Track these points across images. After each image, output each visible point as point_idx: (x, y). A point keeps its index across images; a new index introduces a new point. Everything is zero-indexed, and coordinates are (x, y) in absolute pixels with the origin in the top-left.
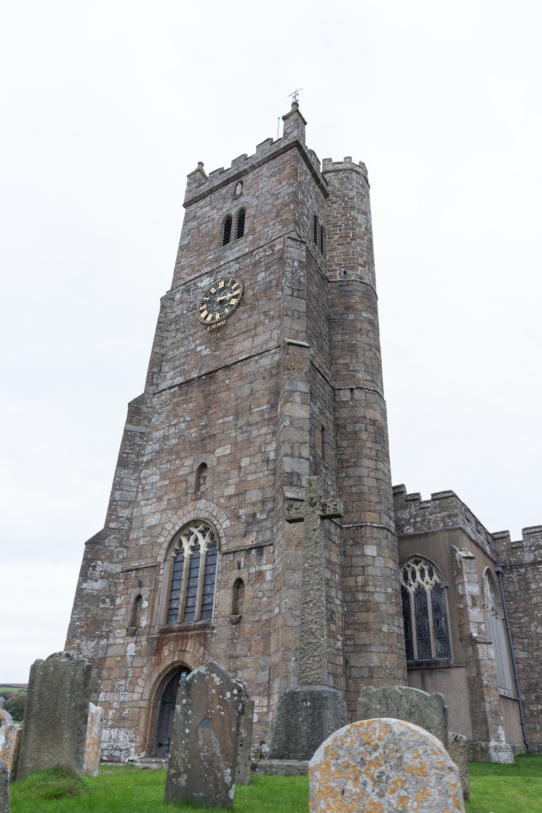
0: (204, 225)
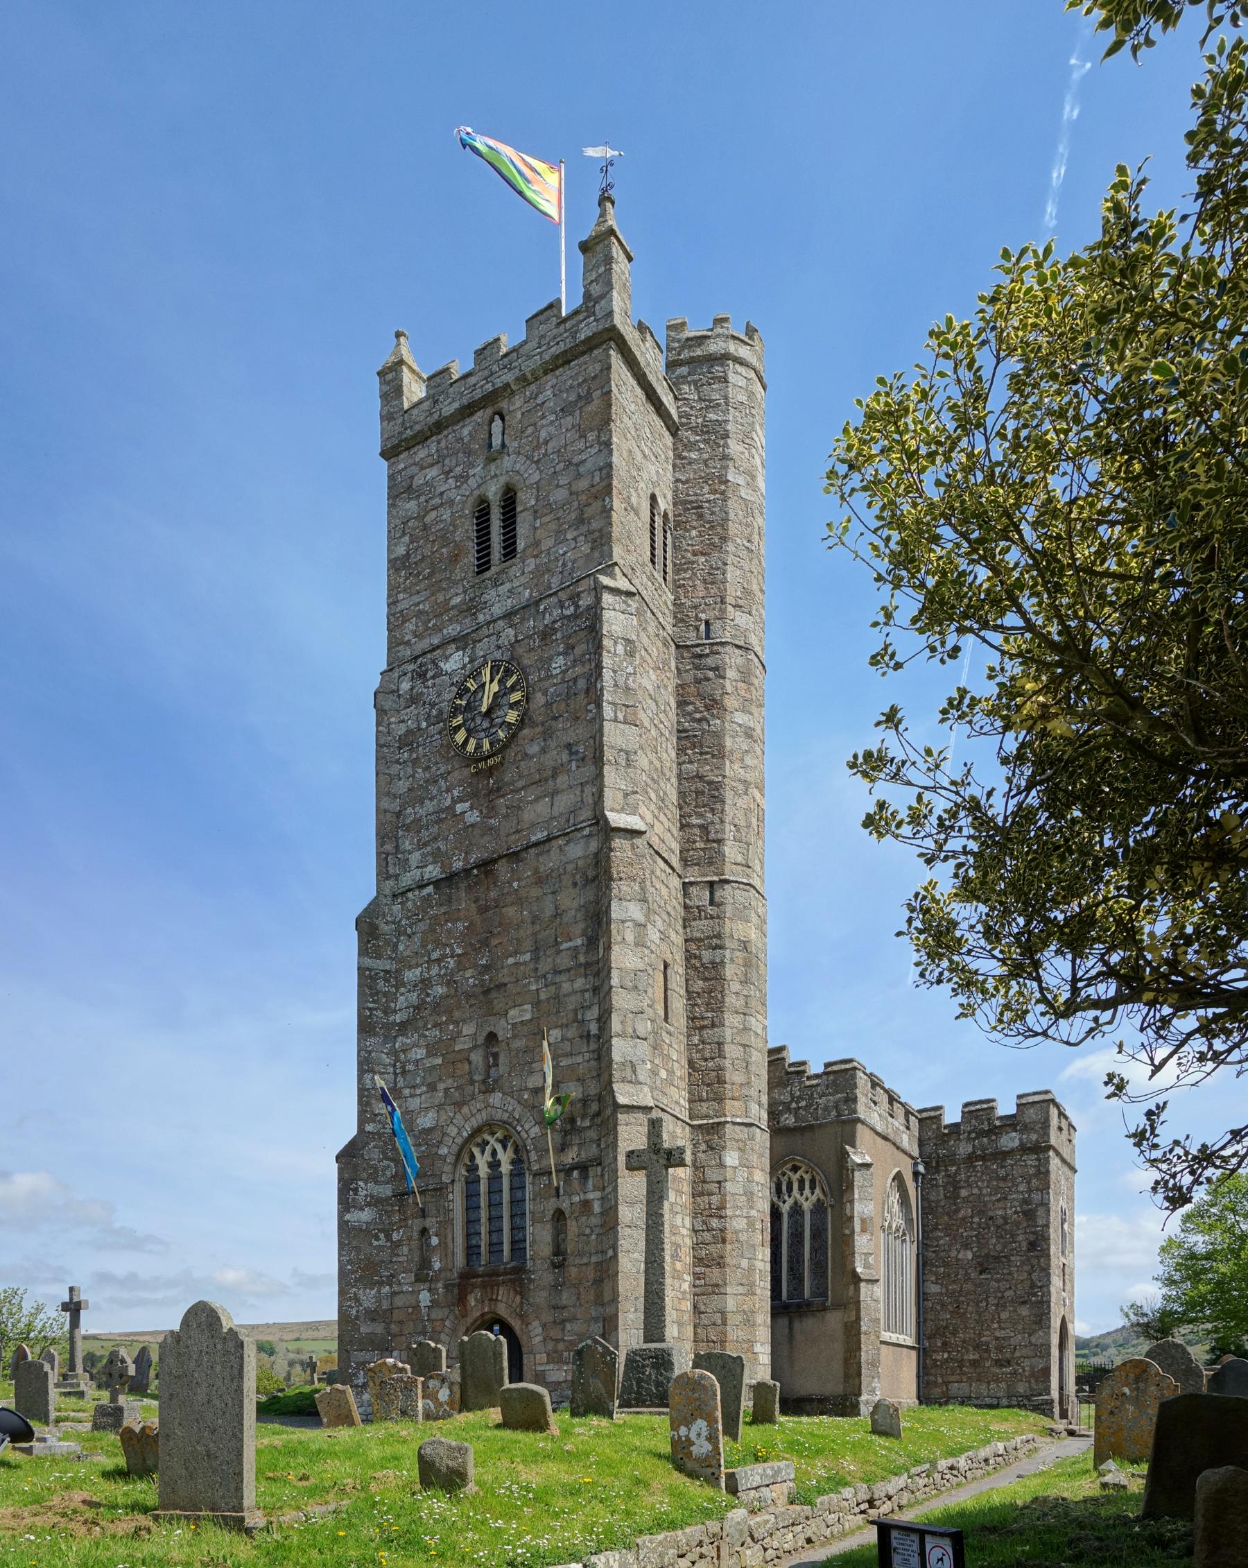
0: (433, 514)
